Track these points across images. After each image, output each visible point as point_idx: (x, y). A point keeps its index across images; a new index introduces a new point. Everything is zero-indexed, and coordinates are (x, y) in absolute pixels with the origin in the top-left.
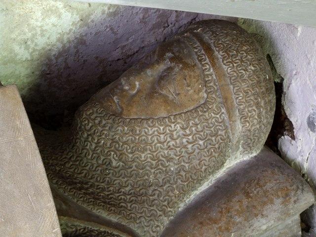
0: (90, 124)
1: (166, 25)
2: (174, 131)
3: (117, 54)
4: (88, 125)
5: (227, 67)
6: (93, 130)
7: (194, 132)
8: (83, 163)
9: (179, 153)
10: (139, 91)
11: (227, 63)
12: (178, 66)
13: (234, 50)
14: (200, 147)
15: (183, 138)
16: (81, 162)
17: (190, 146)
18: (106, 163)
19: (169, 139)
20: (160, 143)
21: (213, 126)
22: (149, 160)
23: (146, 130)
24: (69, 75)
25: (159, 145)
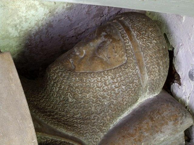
0: (56, 76)
1: (102, 15)
3: (72, 33)
4: (54, 76)
5: (139, 41)
6: (57, 80)
7: (119, 81)
8: (51, 100)
9: (110, 94)
10: (85, 56)
11: (139, 38)
12: (109, 40)
13: (143, 31)
14: (123, 90)
15: (113, 84)
17: (116, 89)
18: (65, 100)
19: (104, 85)
20: (98, 87)
21: (131, 77)
22: (91, 98)
23: (90, 80)
24: (42, 46)
25: (97, 89)
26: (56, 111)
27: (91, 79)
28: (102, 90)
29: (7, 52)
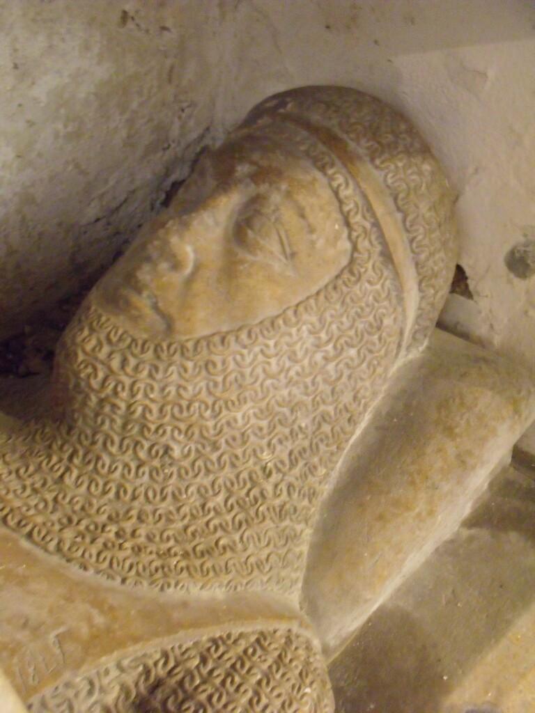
0: (101, 375)
1: (166, 145)
2: (296, 343)
3: (92, 211)
4: (96, 376)
5: (383, 173)
6: (111, 387)
7: (336, 332)
8: (103, 466)
9: (311, 389)
10: (197, 268)
11: (382, 162)
12: (278, 189)
13: (387, 133)
14: (350, 363)
15: (315, 352)
16: (99, 465)
17: (331, 367)
18: (157, 453)
19: (288, 364)
20: (273, 377)
21: (373, 309)
22: (253, 421)
23: (238, 358)
24: (18, 266)
25: (268, 382)
26: (136, 504)
27: (242, 355)
28: (284, 381)
29: (189, 176)
